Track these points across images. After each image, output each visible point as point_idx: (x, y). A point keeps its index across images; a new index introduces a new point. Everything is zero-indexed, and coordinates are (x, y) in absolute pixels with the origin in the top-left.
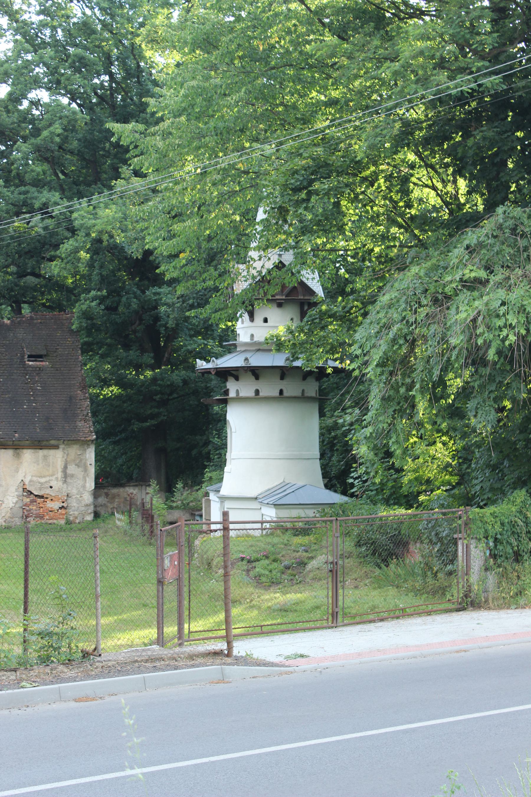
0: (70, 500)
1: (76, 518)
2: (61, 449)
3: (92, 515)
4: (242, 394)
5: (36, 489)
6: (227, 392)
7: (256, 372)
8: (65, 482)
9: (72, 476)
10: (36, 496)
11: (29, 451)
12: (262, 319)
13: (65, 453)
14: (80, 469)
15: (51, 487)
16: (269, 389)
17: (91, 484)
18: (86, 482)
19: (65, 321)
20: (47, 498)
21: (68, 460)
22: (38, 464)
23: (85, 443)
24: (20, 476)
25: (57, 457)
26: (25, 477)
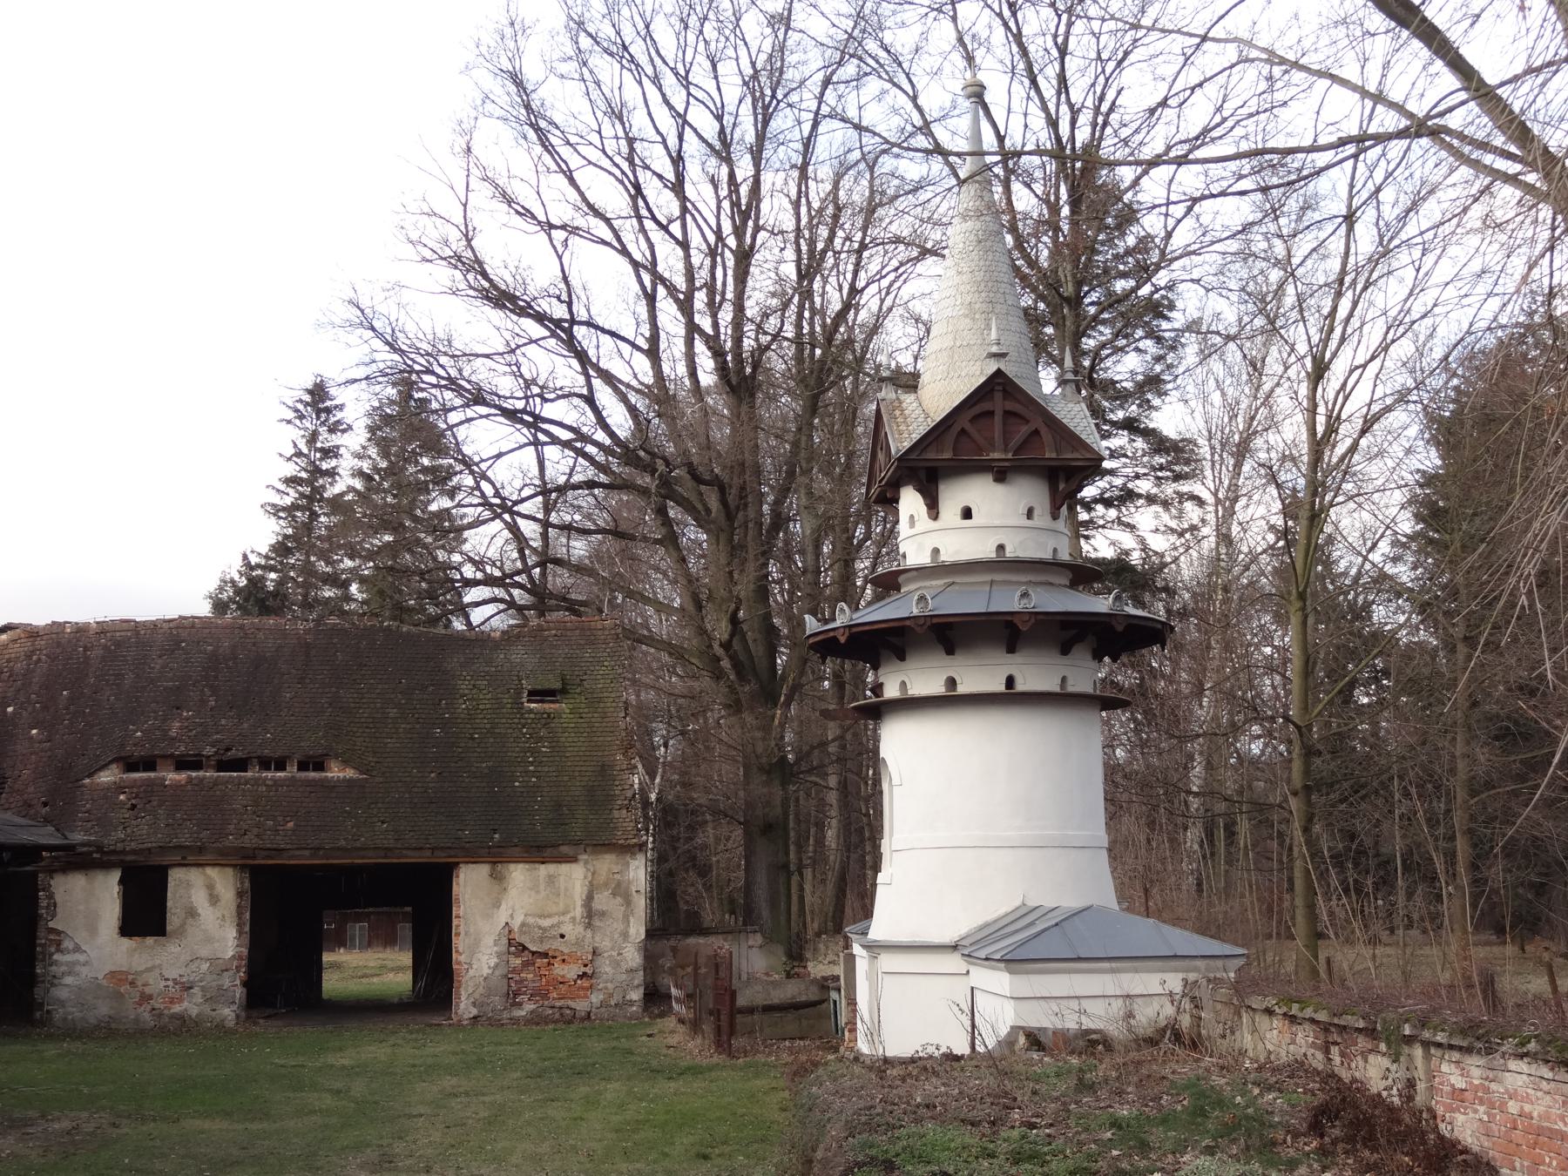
0: (599, 961)
3: (642, 990)
4: (962, 689)
5: (533, 941)
6: (878, 689)
7: (949, 635)
8: (589, 925)
9: (603, 914)
10: (534, 953)
11: (521, 866)
15: (562, 936)
16: (1036, 674)
17: (638, 930)
22: (538, 892)
24: (502, 916)
25: (574, 877)
26: (512, 916)
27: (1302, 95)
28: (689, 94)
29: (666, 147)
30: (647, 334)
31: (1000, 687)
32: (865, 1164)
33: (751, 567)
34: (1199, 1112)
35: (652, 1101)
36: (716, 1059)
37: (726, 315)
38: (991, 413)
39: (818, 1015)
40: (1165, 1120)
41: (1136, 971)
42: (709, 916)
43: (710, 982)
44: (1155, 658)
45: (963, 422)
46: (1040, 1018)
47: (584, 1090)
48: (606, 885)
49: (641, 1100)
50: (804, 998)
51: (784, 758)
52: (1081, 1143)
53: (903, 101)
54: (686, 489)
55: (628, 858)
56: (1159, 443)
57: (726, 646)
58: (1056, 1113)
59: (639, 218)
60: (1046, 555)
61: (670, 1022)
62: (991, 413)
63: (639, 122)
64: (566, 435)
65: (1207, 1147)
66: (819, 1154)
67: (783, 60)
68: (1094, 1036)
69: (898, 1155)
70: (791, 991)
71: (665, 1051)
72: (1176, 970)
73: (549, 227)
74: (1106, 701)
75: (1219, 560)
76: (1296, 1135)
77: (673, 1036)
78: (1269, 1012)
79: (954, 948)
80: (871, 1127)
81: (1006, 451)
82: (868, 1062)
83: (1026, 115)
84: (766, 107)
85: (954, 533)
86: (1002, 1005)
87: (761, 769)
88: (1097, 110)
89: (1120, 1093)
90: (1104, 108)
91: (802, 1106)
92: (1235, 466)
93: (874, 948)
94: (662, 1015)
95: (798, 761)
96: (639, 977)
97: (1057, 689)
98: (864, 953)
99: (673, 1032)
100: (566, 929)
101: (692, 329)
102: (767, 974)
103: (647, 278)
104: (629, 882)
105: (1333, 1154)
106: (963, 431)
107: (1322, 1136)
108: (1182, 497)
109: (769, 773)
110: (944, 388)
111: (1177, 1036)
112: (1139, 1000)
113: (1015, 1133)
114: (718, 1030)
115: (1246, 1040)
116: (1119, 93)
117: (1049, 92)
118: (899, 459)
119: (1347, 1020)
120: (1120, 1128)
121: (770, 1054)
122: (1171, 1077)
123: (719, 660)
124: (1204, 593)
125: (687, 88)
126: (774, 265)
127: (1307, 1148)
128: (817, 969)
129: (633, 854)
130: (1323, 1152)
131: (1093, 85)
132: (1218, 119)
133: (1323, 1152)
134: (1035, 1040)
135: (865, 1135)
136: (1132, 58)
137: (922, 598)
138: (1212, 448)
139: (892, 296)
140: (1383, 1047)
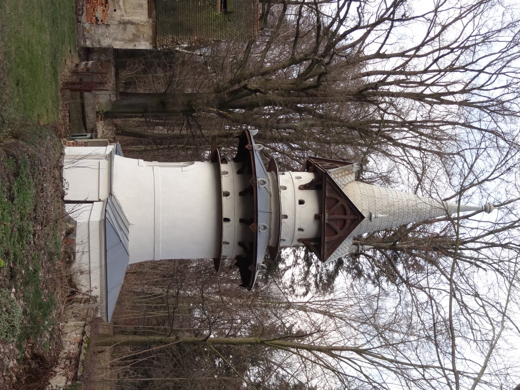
0: (104, 27)
1: (88, 32)
2: (148, 20)
4: (224, 199)
6: (225, 161)
7: (248, 193)
8: (120, 23)
9: (125, 29)
12: (302, 199)
13: (145, 23)
14: (131, 37)
15: (115, 10)
17: (118, 45)
18: (120, 41)
19: (252, 29)
20: (105, 6)
21: (139, 26)
23: (154, 41)
27: (478, 349)
28: (493, 74)
29: (470, 64)
30: (386, 53)
31: (225, 215)
32: (17, 164)
33: (281, 99)
34: (41, 306)
35: (42, 56)
36: (61, 82)
37: (394, 89)
38: (345, 214)
39: (80, 128)
40: (37, 293)
42: (125, 74)
43: (95, 80)
44: (235, 275)
45: (342, 202)
46: (80, 235)
47: (46, 24)
48: (138, 31)
49: (42, 51)
50: (88, 121)
51: (194, 111)
52: (27, 256)
53: (487, 175)
54: (316, 69)
55: (150, 41)
56: (332, 277)
57: (245, 87)
58: (40, 245)
59: (440, 49)
60: (282, 236)
61: (76, 61)
62: (345, 214)
63: (482, 50)
64: (342, 14)
65: (26, 311)
66: (21, 142)
68: (72, 257)
69: (21, 178)
70: (91, 116)
71: (64, 59)
72: (101, 292)
73: (436, 11)
74: (217, 260)
75: (279, 303)
76: (32, 348)
77: (70, 62)
78: (84, 333)
79: (111, 194)
80: (33, 166)
81: (329, 220)
82: (61, 159)
83: (477, 228)
84: (486, 107)
85: (293, 194)
86: (86, 218)
87: (190, 101)
88: (477, 259)
89: (49, 272)
90: (478, 263)
91: (41, 132)
92: (320, 311)
93: (110, 158)
94: (79, 56)
95: (193, 117)
96: (96, 45)
97: (224, 240)
98: (108, 153)
99: (72, 62)
100: (118, 12)
101: (389, 74)
102: (98, 103)
103: (412, 53)
104: (139, 42)
105: (24, 364)
106: (338, 201)
107: (32, 359)
108: (308, 286)
109: (188, 105)
110: (357, 193)
111: (73, 293)
112: (88, 276)
113: (31, 229)
114: (73, 84)
115: (72, 323)
116: (485, 269)
117: (488, 239)
118: (326, 173)
119: (81, 368)
120: (34, 273)
121: (63, 107)
122: (56, 293)
123: (239, 83)
124: (267, 297)
125: (495, 73)
126: (416, 112)
127: (26, 352)
128: (101, 127)
129: (152, 44)
130: (25, 359)
131: (489, 258)
132: (470, 311)
133: (25, 359)
134: (71, 232)
135: (29, 163)
136: (499, 276)
137: (264, 183)
138: (329, 301)
139: (400, 161)
140: (69, 383)
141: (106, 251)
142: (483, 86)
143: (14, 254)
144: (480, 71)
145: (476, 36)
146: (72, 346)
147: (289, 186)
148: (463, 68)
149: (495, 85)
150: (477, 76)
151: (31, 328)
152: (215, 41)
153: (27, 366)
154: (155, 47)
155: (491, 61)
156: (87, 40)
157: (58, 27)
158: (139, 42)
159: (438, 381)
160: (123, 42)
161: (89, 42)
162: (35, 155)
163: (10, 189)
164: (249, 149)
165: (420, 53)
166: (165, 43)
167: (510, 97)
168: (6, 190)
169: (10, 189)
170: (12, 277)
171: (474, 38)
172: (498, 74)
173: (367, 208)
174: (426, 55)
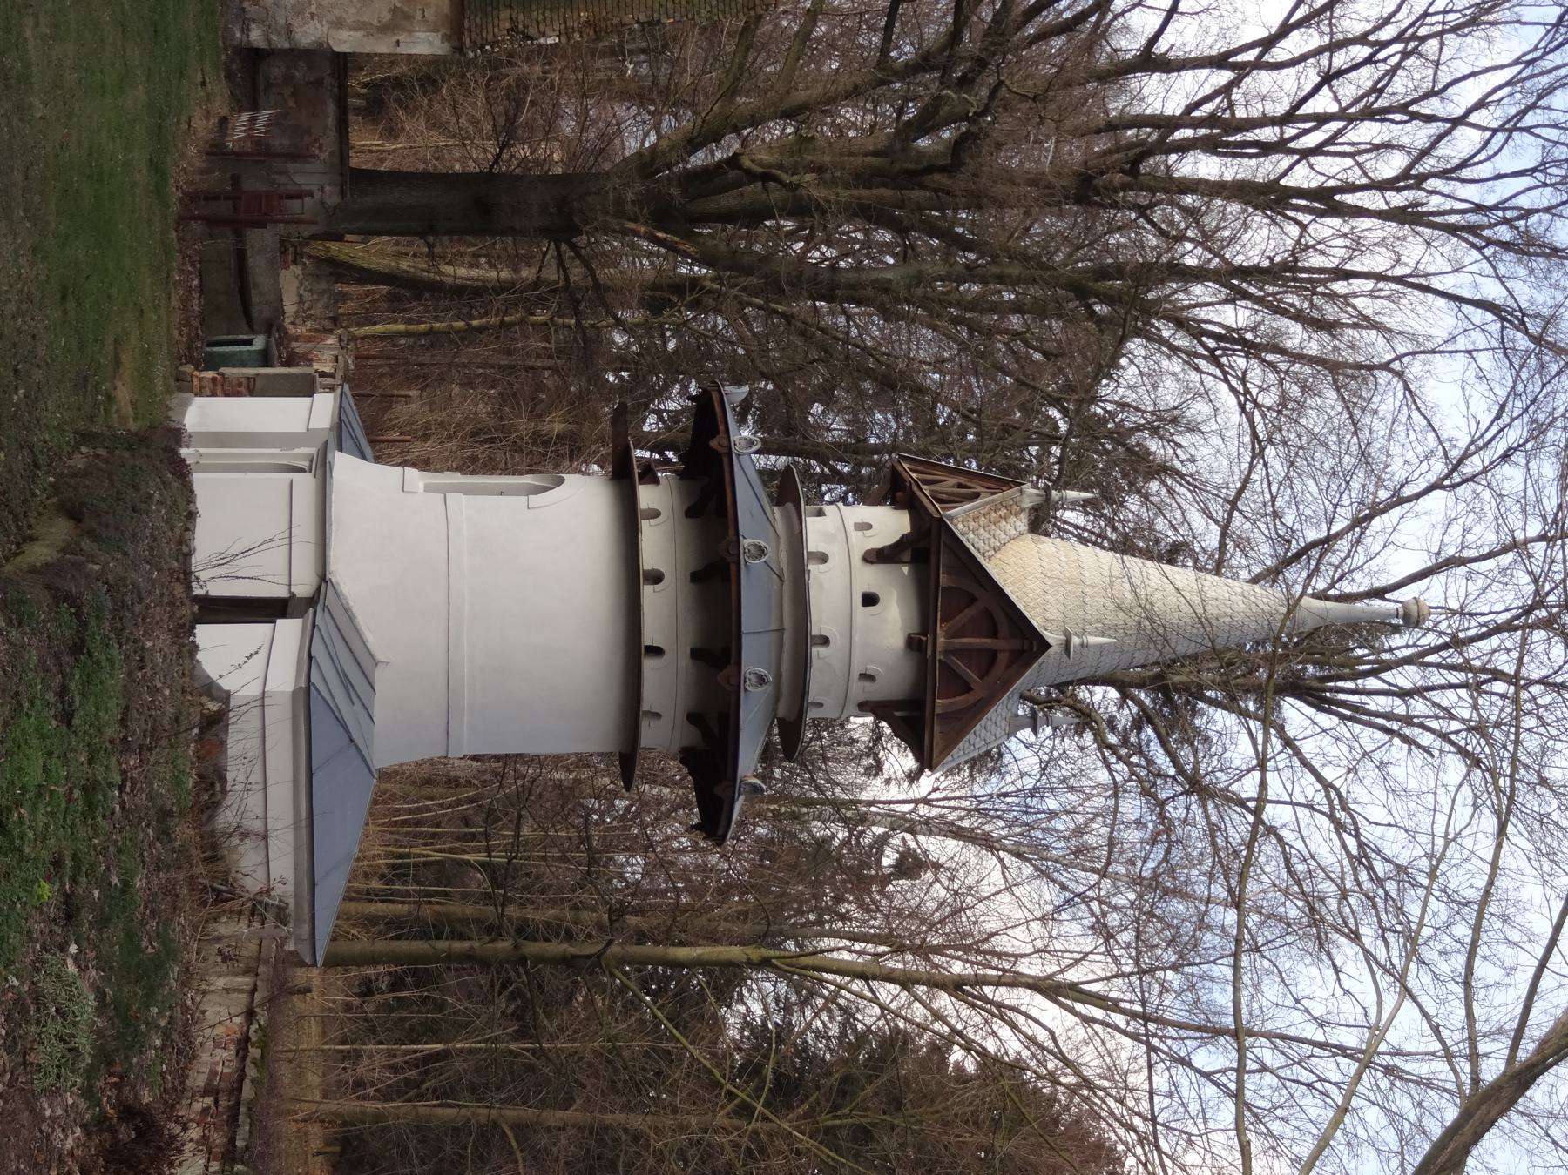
3: (263, 45)
4: (647, 591)
6: (649, 475)
7: (715, 575)
14: (387, 17)
16: (664, 684)
17: (345, 41)
18: (352, 29)
28: (1495, 131)
29: (1426, 96)
31: (650, 637)
36: (174, 195)
41: (297, 849)
46: (239, 741)
50: (255, 299)
60: (813, 696)
62: (994, 634)
67: (1537, 255)
68: (218, 786)
69: (90, 654)
79: (323, 578)
84: (1473, 229)
88: (1408, 720)
96: (281, 42)
97: (645, 707)
103: (1250, 56)
104: (410, 32)
114: (211, 197)
118: (941, 520)
120: (123, 891)
125: (1501, 129)
133: (101, 1121)
137: (761, 551)
141: (310, 774)
142: (1464, 164)
143: (74, 857)
144: (1458, 122)
145: (1445, 12)
146: (223, 1054)
147: (835, 551)
148: (1403, 108)
149: (1505, 163)
150: (1448, 132)
151: (117, 1038)
152: (642, 24)
153: (106, 1135)
154: (460, 49)
155: (1489, 88)
156: (253, 26)
157: (167, 41)
158: (410, 32)
159: (1279, 1077)
160: (359, 34)
161: (259, 32)
162: (124, 579)
163: (63, 691)
164: (720, 450)
165: (1279, 53)
166: (490, 37)
167: (1545, 197)
168: (52, 700)
169: (63, 691)
170: (69, 917)
171: (1439, 18)
172: (1511, 131)
173: (1060, 616)
174: (1293, 63)
